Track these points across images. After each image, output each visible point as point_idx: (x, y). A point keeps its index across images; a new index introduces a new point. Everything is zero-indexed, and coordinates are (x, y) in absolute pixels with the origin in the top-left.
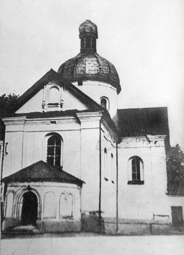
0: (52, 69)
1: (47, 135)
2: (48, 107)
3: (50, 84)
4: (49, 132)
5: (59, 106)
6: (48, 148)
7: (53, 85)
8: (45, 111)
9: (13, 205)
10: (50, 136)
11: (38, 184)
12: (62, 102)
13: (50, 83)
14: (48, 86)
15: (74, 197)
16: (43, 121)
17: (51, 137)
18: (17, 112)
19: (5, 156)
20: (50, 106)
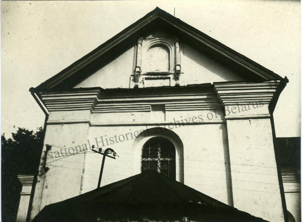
0: (157, 7)
1: (144, 134)
2: (146, 79)
3: (149, 39)
4: (145, 128)
5: (171, 76)
6: (143, 162)
7: (157, 40)
8: (141, 86)
9: (214, 99)
10: (146, 139)
11: (41, 207)
12: (178, 68)
13: (151, 37)
14: (145, 44)
15: (39, 209)
16: (132, 113)
17: (151, 139)
18: (78, 86)
19: (42, 175)
20: (150, 76)
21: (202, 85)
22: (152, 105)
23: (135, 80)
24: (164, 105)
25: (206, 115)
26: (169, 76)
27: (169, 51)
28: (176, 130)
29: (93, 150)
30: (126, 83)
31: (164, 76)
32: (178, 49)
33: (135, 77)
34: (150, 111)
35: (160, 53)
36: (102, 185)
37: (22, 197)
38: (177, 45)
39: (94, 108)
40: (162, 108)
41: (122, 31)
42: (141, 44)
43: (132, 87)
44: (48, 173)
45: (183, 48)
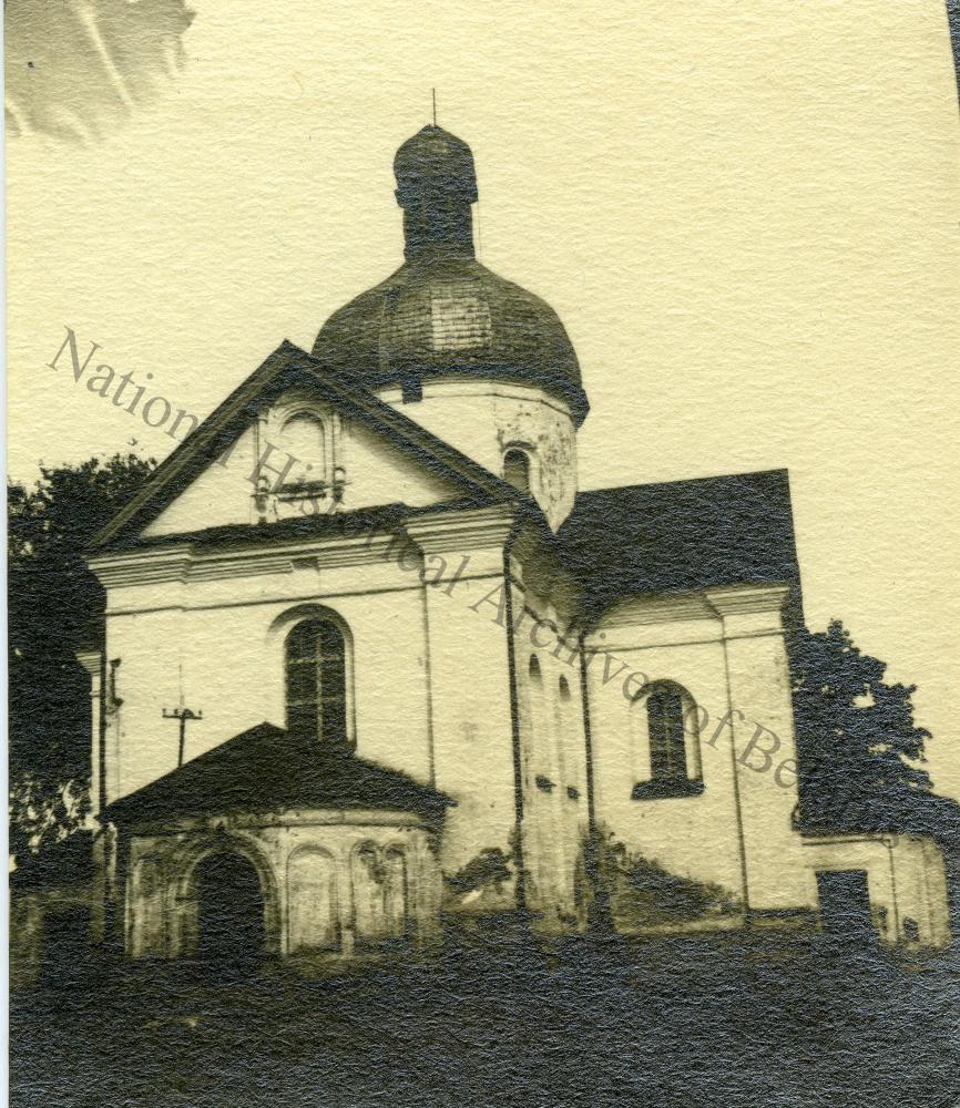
1: (281, 619)
3: (281, 404)
7: (298, 405)
8: (271, 519)
13: (284, 398)
17: (296, 627)
21: (198, 766)
22: (294, 561)
23: (261, 507)
24: (315, 557)
25: (389, 573)
26: (325, 490)
27: (322, 428)
28: (342, 607)
29: (164, 716)
30: (246, 515)
31: (313, 490)
32: (337, 431)
33: (259, 499)
34: (291, 572)
35: (304, 433)
36: (187, 759)
37: (110, 621)
38: (336, 417)
39: (187, 573)
40: (310, 562)
41: (184, 535)
42: (266, 422)
43: (254, 521)
44: (123, 710)
45: (350, 426)
